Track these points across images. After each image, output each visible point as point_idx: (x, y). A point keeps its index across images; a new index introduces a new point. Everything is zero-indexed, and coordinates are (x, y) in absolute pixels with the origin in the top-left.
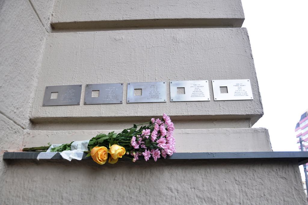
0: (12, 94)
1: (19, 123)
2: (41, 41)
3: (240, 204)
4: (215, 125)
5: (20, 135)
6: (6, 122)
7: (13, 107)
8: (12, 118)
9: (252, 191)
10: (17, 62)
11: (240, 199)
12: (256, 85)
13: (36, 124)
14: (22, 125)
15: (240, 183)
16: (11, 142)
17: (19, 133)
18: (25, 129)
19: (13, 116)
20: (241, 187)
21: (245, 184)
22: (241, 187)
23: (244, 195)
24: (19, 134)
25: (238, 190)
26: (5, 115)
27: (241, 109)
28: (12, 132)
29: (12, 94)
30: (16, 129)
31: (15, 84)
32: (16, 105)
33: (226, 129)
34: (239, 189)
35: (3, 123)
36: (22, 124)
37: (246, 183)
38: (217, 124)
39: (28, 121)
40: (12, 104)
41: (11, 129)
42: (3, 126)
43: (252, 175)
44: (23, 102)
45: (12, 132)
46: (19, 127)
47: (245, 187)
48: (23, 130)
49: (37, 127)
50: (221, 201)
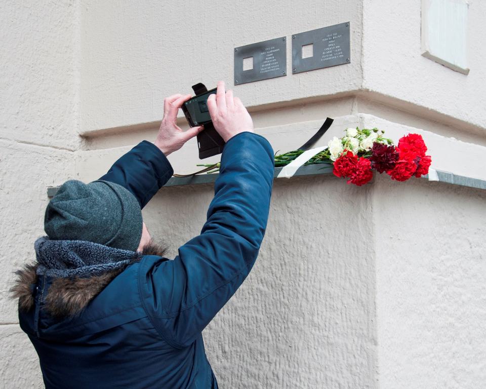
0: (39, 113)
1: (63, 146)
2: (70, 7)
3: (290, 240)
4: (303, 114)
5: (68, 162)
6: (39, 152)
7: (46, 129)
8: (48, 144)
9: (306, 222)
10: (33, 69)
11: (290, 233)
12: (359, 32)
13: (92, 139)
14: (68, 148)
15: (292, 210)
16: (55, 174)
17: (67, 159)
18: (75, 150)
19: (49, 141)
20: (294, 217)
21: (299, 212)
22: (294, 217)
23: (297, 227)
24: (67, 160)
25: (289, 221)
26: (35, 144)
27: (330, 84)
28: (53, 161)
29: (39, 113)
30: (58, 156)
31: (39, 99)
32: (49, 125)
33: (303, 122)
34: (291, 220)
35: (36, 154)
36: (68, 145)
37: (300, 210)
38: (303, 110)
39: (78, 139)
40: (43, 127)
41: (50, 158)
42: (37, 158)
43: (308, 199)
44: (62, 116)
45: (53, 161)
46: (65, 150)
47: (299, 216)
48: (71, 153)
49: (94, 143)
50: (269, 236)
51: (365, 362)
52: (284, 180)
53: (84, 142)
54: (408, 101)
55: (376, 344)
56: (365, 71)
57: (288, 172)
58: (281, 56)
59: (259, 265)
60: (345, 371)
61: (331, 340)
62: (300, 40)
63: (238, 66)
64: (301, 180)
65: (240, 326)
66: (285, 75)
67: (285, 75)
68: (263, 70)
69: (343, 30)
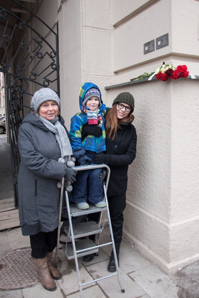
39: (113, 73)
49: (118, 74)
51: (169, 132)
52: (150, 81)
53: (115, 74)
54: (192, 54)
55: (171, 127)
56: (172, 47)
57: (150, 79)
58: (154, 45)
59: (136, 110)
60: (165, 134)
61: (162, 126)
62: (158, 39)
63: (145, 49)
64: (153, 81)
65: (143, 122)
66: (154, 50)
67: (154, 50)
68: (150, 50)
69: (167, 36)
